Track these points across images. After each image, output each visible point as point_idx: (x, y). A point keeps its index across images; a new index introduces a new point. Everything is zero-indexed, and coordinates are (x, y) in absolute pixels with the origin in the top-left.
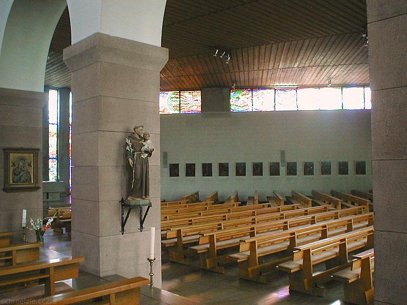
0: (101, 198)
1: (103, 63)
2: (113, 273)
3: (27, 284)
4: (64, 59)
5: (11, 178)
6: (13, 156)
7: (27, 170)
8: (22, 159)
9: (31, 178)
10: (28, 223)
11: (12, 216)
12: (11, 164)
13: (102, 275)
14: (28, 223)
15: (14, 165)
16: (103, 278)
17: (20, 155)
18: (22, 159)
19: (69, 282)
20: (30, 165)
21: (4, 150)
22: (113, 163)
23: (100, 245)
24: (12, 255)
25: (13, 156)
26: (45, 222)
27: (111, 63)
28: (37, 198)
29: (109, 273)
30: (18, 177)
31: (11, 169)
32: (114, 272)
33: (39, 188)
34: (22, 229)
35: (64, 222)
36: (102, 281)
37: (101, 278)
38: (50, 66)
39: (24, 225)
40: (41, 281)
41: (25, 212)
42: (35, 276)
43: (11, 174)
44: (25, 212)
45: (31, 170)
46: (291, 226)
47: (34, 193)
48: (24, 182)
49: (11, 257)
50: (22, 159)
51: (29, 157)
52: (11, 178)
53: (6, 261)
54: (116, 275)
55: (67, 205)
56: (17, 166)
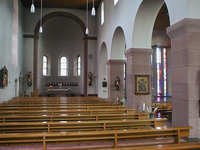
0: (189, 99)
1: (189, 33)
2: (195, 137)
3: (33, 143)
4: (167, 33)
5: (138, 89)
6: (139, 79)
7: (145, 85)
8: (143, 80)
9: (146, 89)
10: (146, 109)
11: (138, 106)
12: (138, 82)
13: (189, 137)
14: (146, 109)
15: (139, 83)
16: (190, 139)
17: (141, 78)
18: (142, 80)
19: (7, 145)
20: (146, 83)
21: (135, 76)
22: (195, 82)
23: (189, 122)
24: (154, 123)
25: (139, 79)
26: (153, 109)
27: (193, 32)
28: (149, 98)
29: (193, 137)
30: (141, 88)
31: (138, 85)
32: (196, 136)
33: (150, 93)
34: (143, 112)
35: (160, 110)
36: (189, 140)
37: (189, 139)
38: (154, 36)
39: (144, 110)
40: (173, 136)
41: (144, 104)
42: (159, 134)
43: (138, 86)
44: (144, 104)
45: (146, 85)
46: (102, 129)
47: (148, 96)
48: (143, 90)
49: (154, 124)
50: (142, 80)
51: (145, 79)
52: (138, 89)
53: (151, 125)
54: (196, 138)
55: (163, 102)
56: (140, 83)
